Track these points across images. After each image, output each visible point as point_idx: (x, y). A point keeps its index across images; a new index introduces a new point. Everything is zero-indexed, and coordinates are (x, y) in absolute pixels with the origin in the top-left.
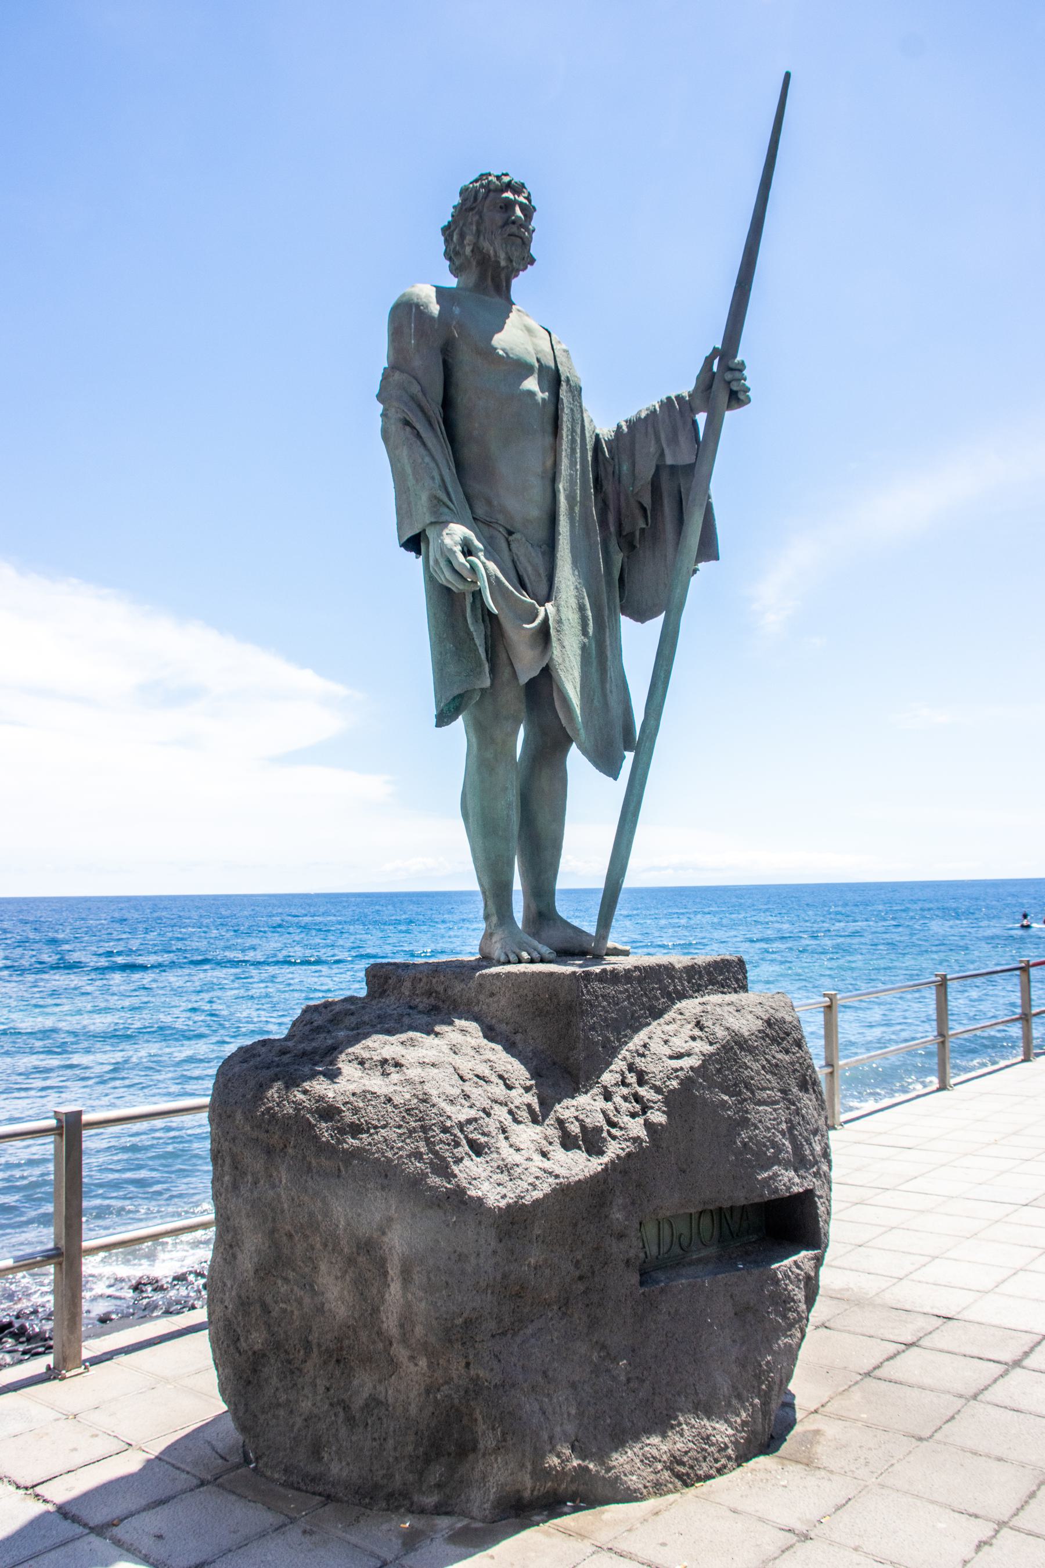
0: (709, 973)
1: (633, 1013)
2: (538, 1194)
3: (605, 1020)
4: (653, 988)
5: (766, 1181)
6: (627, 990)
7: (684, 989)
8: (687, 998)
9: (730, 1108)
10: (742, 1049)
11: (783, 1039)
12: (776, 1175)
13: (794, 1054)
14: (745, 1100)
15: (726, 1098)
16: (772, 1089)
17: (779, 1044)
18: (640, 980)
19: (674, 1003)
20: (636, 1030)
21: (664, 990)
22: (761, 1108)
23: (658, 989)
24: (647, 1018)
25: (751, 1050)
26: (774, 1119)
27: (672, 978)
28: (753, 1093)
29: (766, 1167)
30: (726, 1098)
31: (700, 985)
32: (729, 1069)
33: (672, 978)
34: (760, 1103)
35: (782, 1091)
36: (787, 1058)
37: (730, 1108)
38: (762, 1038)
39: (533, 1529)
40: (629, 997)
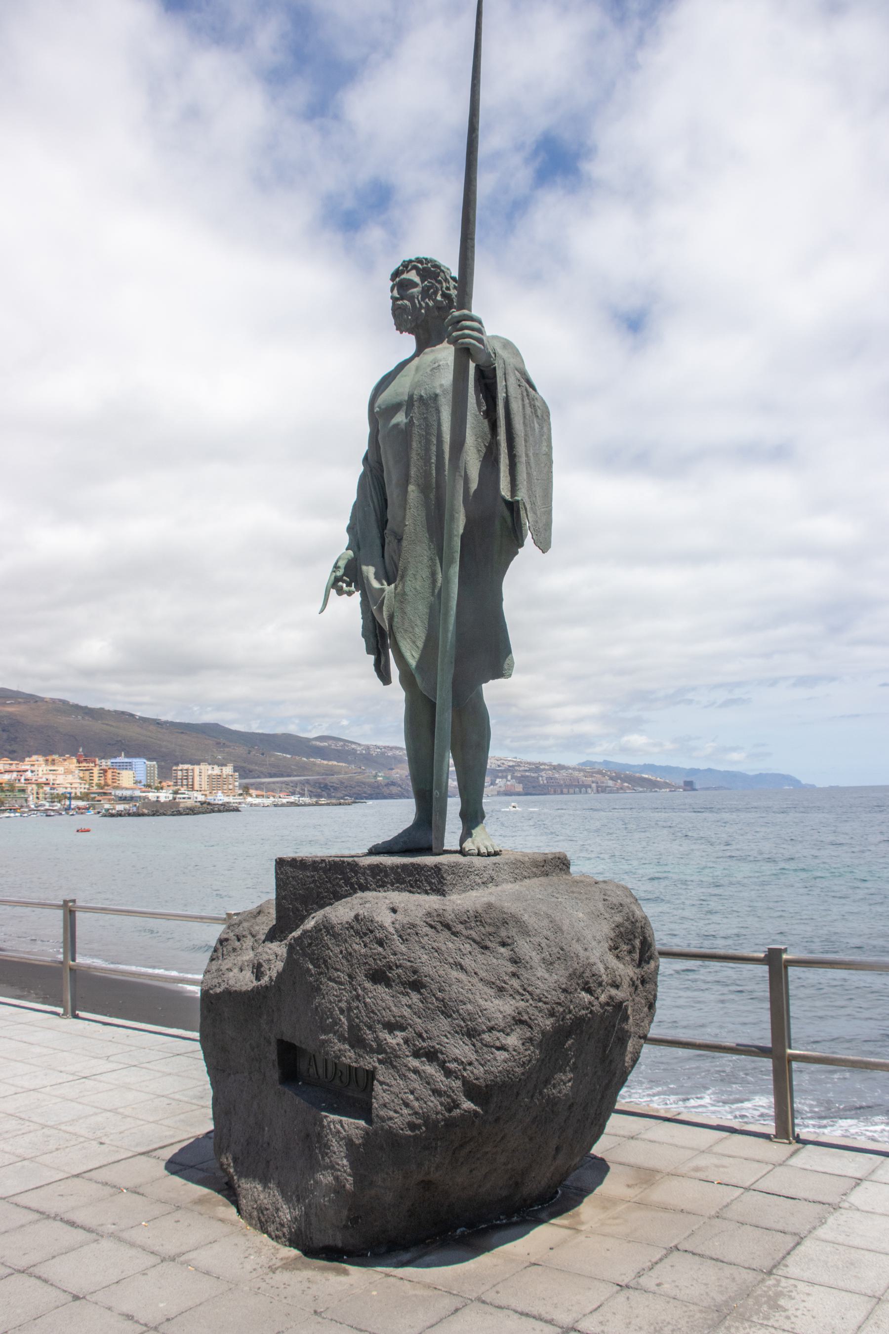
0: (396, 873)
1: (319, 894)
2: (218, 990)
3: (295, 894)
4: (337, 878)
5: (324, 1042)
6: (313, 876)
7: (367, 883)
8: (370, 890)
9: (312, 975)
10: (328, 932)
11: (365, 934)
12: (328, 1041)
13: (371, 949)
14: (321, 973)
15: (311, 967)
16: (343, 972)
17: (361, 937)
18: (325, 871)
19: (355, 892)
20: (322, 907)
21: (347, 881)
22: (331, 984)
23: (341, 879)
24: (331, 899)
25: (335, 936)
26: (337, 996)
27: (356, 873)
28: (328, 969)
29: (325, 1032)
30: (311, 967)
31: (384, 882)
32: (316, 945)
33: (356, 873)
34: (330, 979)
35: (350, 976)
36: (363, 951)
37: (312, 975)
38: (347, 928)
39: (487, 1254)
40: (314, 881)
